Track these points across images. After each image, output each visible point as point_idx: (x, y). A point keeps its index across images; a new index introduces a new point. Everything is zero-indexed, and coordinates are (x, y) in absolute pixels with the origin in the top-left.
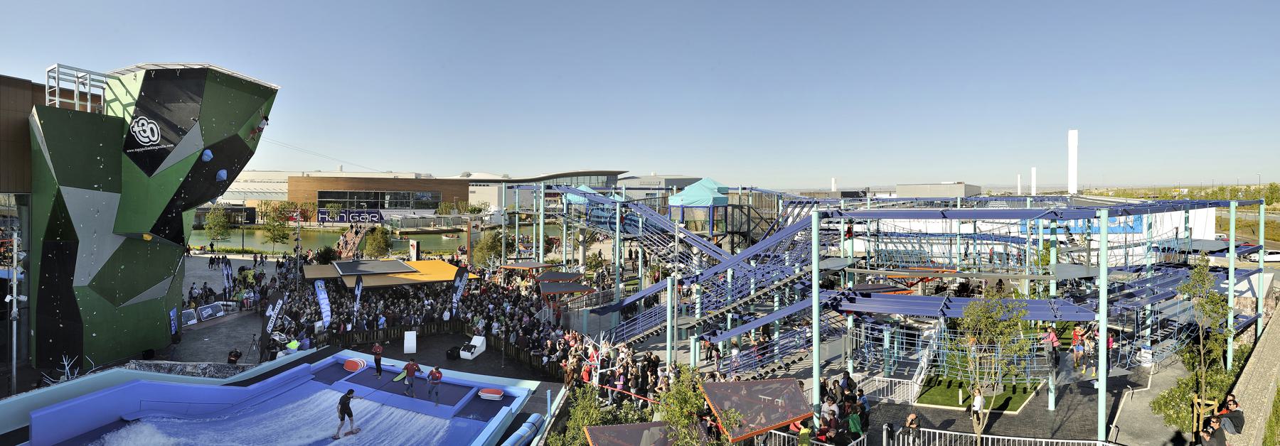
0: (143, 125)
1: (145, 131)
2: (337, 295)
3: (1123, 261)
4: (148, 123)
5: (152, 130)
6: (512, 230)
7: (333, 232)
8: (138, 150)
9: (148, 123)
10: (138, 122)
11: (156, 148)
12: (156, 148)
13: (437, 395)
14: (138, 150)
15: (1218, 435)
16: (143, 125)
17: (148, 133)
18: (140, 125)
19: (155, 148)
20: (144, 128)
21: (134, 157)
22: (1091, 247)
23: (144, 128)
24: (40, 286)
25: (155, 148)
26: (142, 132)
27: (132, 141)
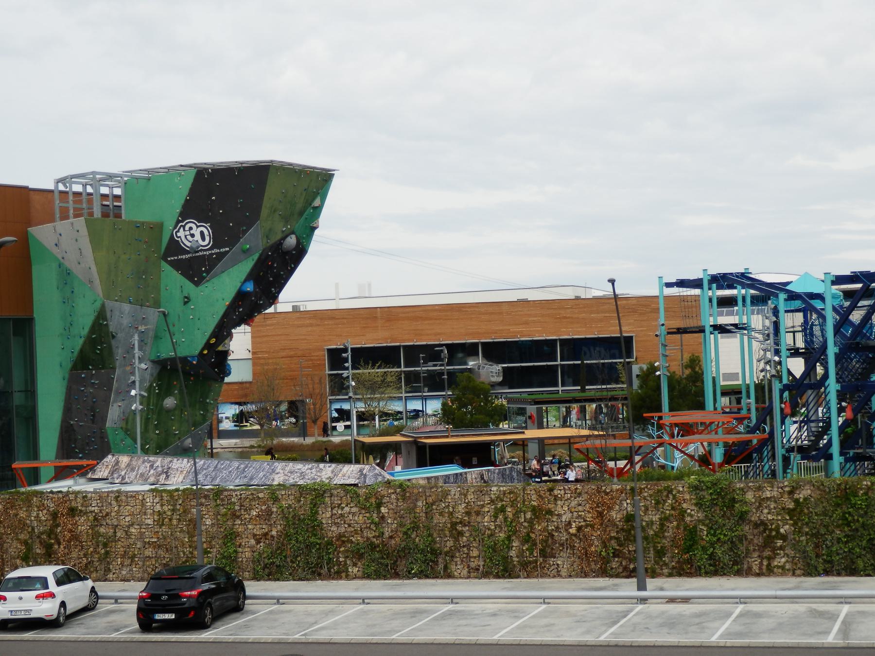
0: (191, 228)
1: (193, 236)
2: (277, 421)
3: (388, 404)
4: (198, 227)
5: (202, 233)
6: (616, 435)
7: (52, 492)
8: (184, 257)
9: (198, 227)
10: (184, 227)
11: (207, 253)
12: (207, 253)
13: (185, 303)
14: (184, 257)
15: (873, 545)
16: (191, 228)
17: (198, 237)
18: (187, 228)
19: (205, 253)
20: (192, 232)
21: (176, 265)
22: (568, 445)
23: (192, 232)
24: (203, 349)
25: (205, 253)
26: (189, 237)
27: (174, 246)
